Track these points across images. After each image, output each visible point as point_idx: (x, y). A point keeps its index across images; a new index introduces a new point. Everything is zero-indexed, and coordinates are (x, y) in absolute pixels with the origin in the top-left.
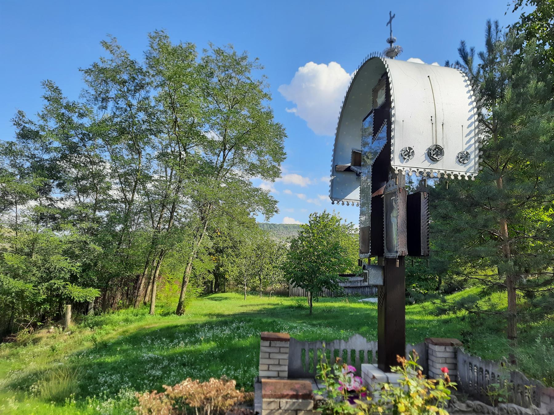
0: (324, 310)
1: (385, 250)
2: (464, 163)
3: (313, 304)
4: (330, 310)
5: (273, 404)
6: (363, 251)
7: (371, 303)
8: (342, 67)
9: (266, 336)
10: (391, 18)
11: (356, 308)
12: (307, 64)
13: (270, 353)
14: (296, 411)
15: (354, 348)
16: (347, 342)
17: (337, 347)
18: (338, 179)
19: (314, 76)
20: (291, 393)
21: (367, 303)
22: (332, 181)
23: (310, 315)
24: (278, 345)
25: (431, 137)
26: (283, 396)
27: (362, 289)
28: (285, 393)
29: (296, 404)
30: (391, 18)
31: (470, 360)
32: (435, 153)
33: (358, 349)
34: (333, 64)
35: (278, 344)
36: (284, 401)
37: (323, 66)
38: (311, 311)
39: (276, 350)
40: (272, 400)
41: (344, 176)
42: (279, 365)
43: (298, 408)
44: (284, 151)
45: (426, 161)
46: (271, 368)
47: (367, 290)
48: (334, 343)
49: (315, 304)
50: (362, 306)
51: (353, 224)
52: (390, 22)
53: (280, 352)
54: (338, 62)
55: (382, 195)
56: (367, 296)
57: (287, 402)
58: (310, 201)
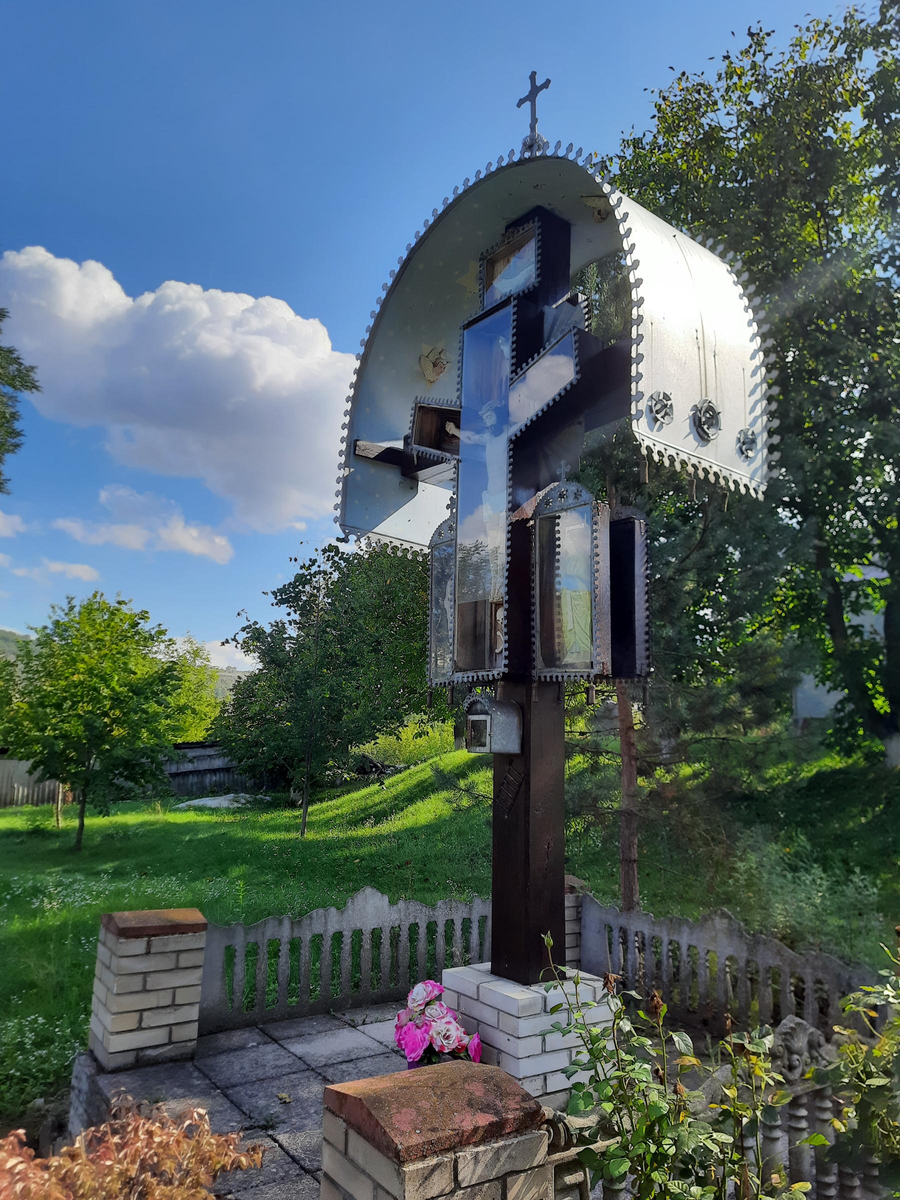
0: (125, 833)
1: (539, 662)
2: (747, 457)
3: (87, 821)
4: (124, 834)
5: (436, 1176)
6: (460, 665)
7: (211, 809)
8: (117, 277)
9: (133, 924)
10: (535, 91)
11: (189, 822)
12: (29, 249)
13: (145, 974)
14: (503, 1181)
15: (359, 925)
16: (342, 912)
17: (318, 928)
18: (358, 478)
19: (44, 282)
20: (484, 1120)
21: (200, 809)
22: (345, 481)
23: (77, 851)
24: (172, 947)
25: (698, 382)
26: (462, 1140)
27: (179, 780)
28: (468, 1126)
29: (504, 1155)
30: (535, 91)
31: (622, 921)
32: (705, 421)
33: (368, 926)
34: (92, 266)
35: (175, 942)
36: (467, 1153)
37: (65, 267)
38: (79, 841)
39: (166, 963)
40: (433, 1161)
41: (372, 471)
42: (174, 1005)
43: (508, 1168)
44: (18, 426)
45: (691, 436)
46: (149, 1019)
47: (192, 779)
48: (311, 918)
49: (94, 822)
50: (190, 817)
51: (163, 628)
52: (532, 97)
53: (177, 968)
54: (108, 265)
55: (528, 520)
56: (192, 795)
57: (476, 1158)
58: (20, 572)
